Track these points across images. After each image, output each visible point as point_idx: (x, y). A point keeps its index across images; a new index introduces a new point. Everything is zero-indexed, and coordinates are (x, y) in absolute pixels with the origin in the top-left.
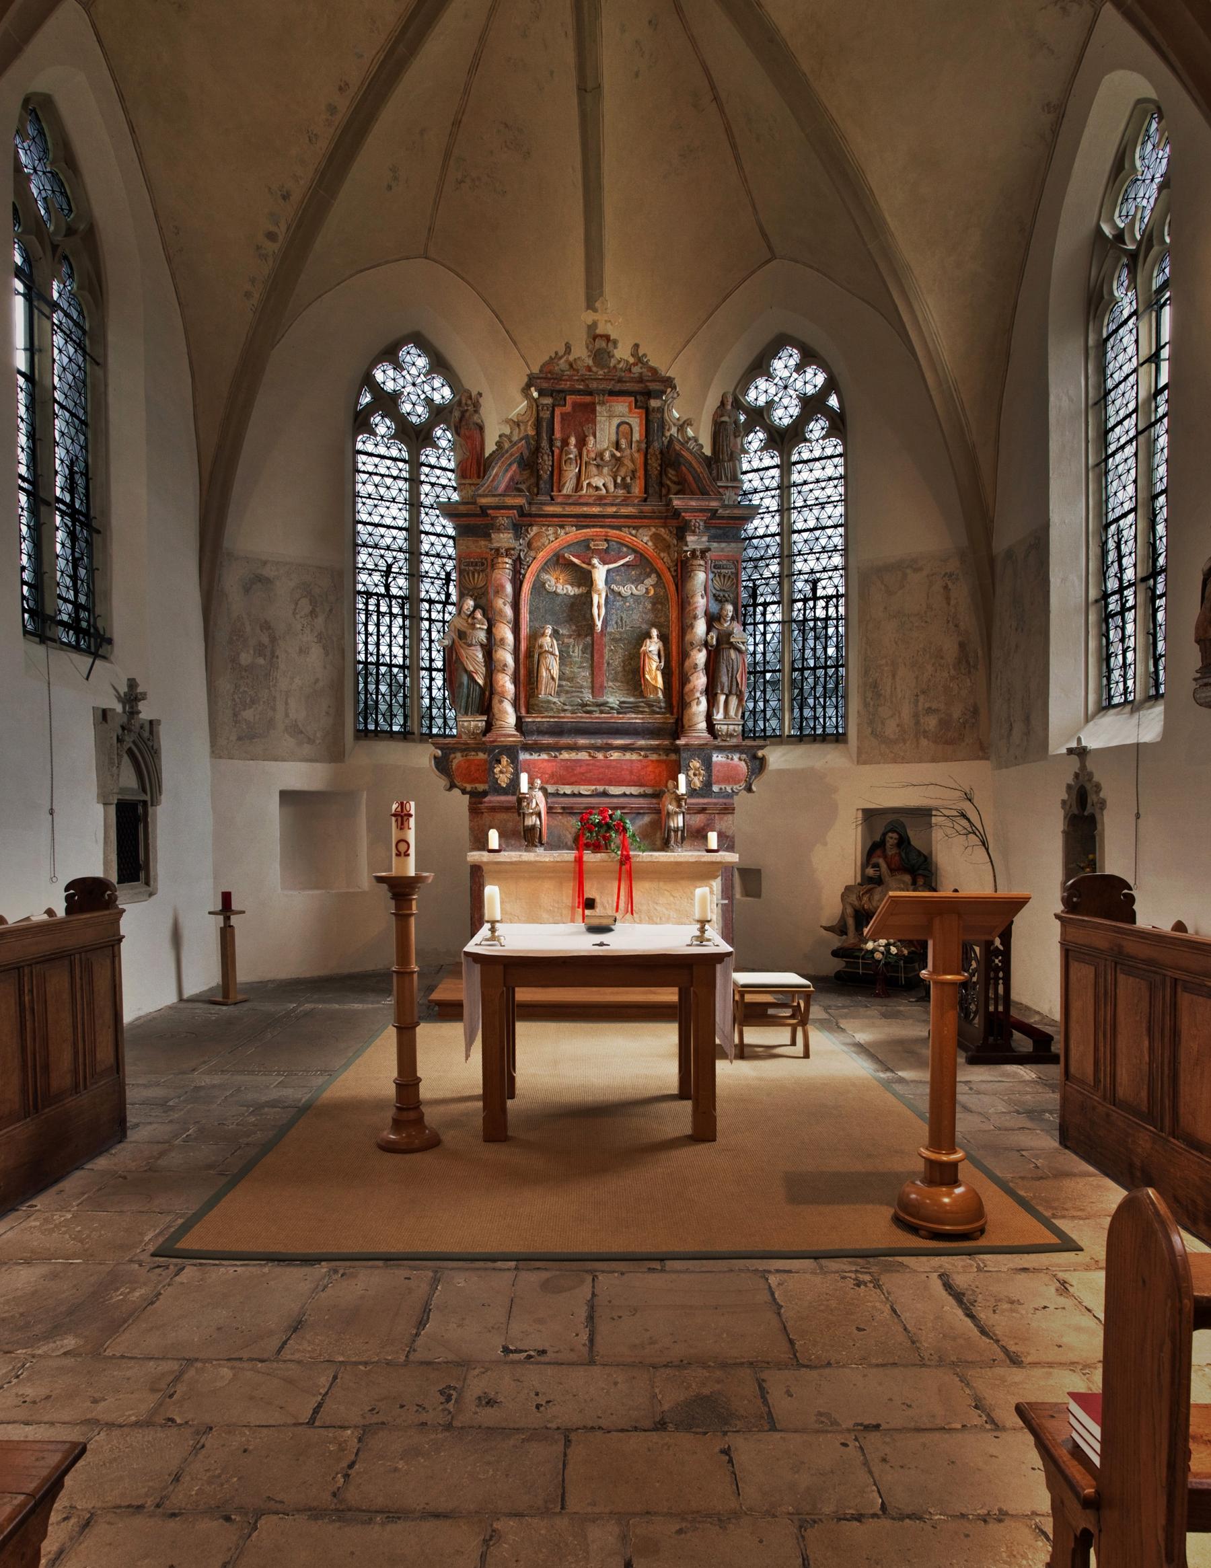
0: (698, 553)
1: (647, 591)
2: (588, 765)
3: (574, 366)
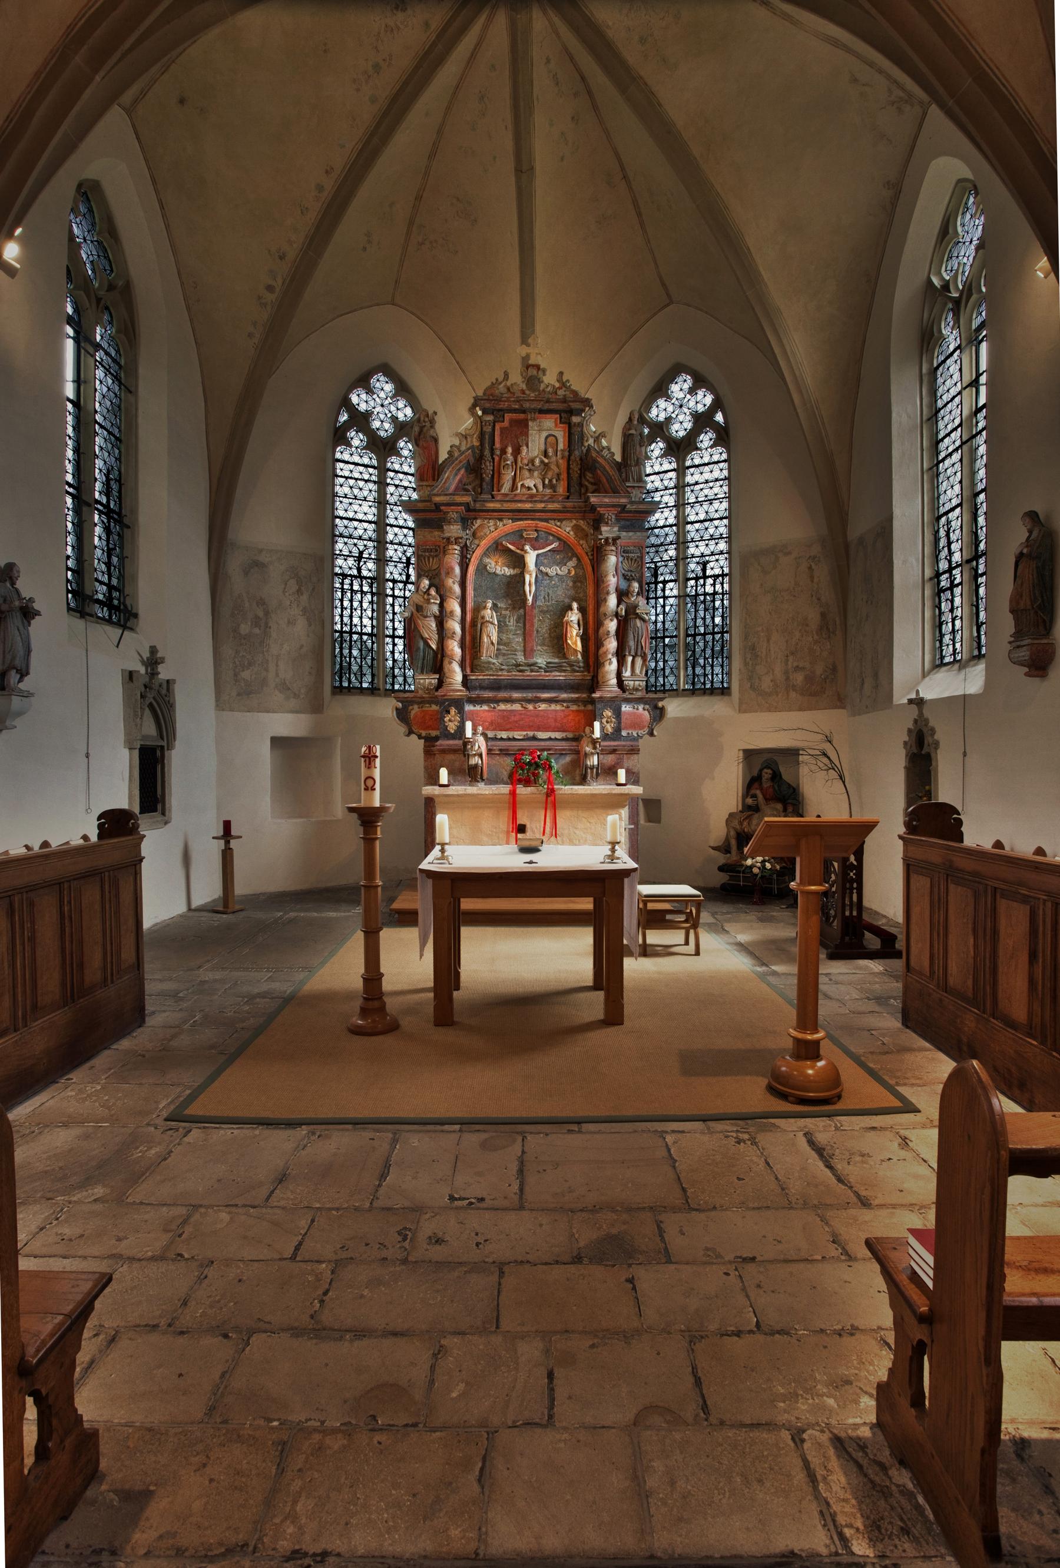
0: (610, 541)
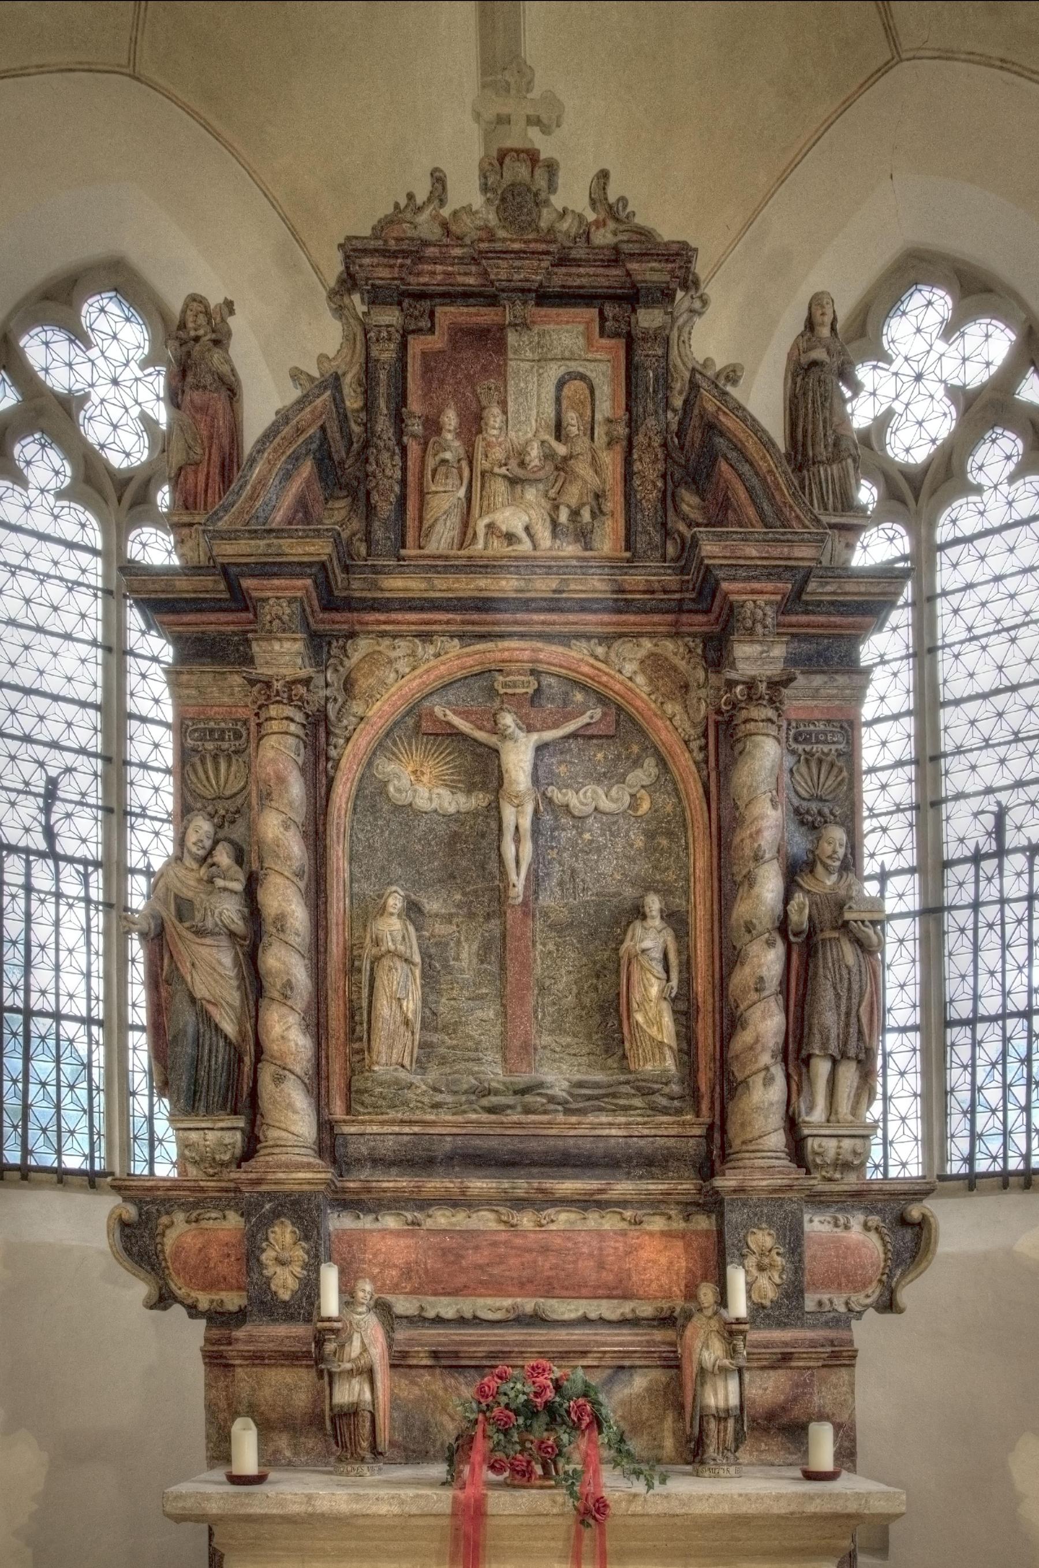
0: (763, 687)
1: (634, 805)
2: (494, 1244)
3: (453, 228)
